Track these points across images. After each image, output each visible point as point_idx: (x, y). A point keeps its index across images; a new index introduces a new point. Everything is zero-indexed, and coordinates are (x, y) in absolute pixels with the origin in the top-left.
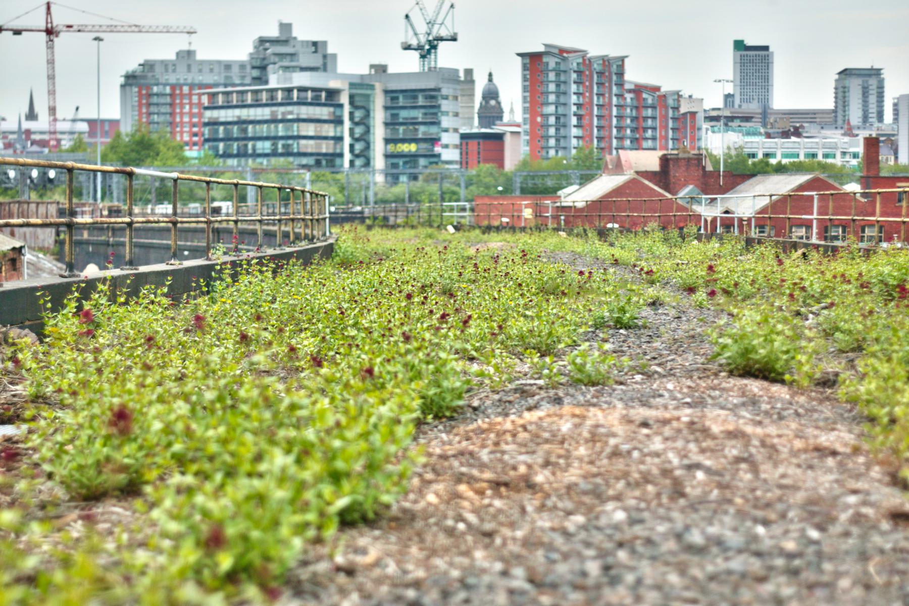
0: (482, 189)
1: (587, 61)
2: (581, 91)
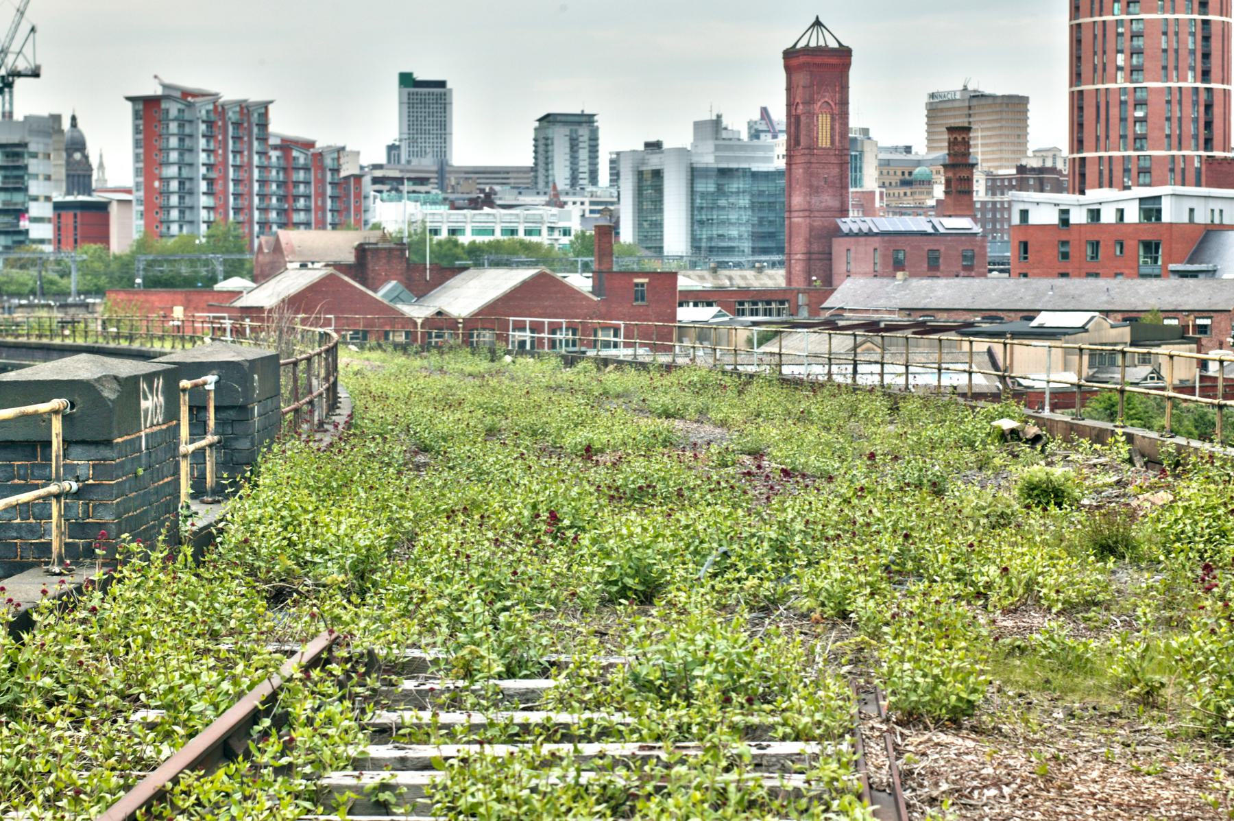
0: (89, 277)
1: (220, 110)
2: (212, 147)
